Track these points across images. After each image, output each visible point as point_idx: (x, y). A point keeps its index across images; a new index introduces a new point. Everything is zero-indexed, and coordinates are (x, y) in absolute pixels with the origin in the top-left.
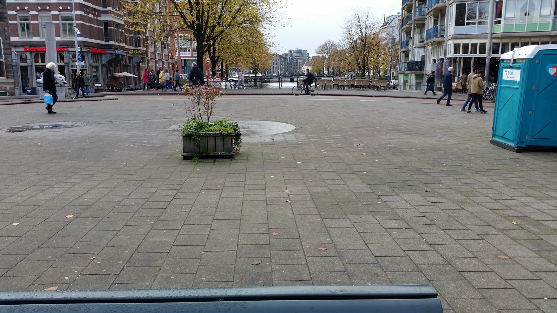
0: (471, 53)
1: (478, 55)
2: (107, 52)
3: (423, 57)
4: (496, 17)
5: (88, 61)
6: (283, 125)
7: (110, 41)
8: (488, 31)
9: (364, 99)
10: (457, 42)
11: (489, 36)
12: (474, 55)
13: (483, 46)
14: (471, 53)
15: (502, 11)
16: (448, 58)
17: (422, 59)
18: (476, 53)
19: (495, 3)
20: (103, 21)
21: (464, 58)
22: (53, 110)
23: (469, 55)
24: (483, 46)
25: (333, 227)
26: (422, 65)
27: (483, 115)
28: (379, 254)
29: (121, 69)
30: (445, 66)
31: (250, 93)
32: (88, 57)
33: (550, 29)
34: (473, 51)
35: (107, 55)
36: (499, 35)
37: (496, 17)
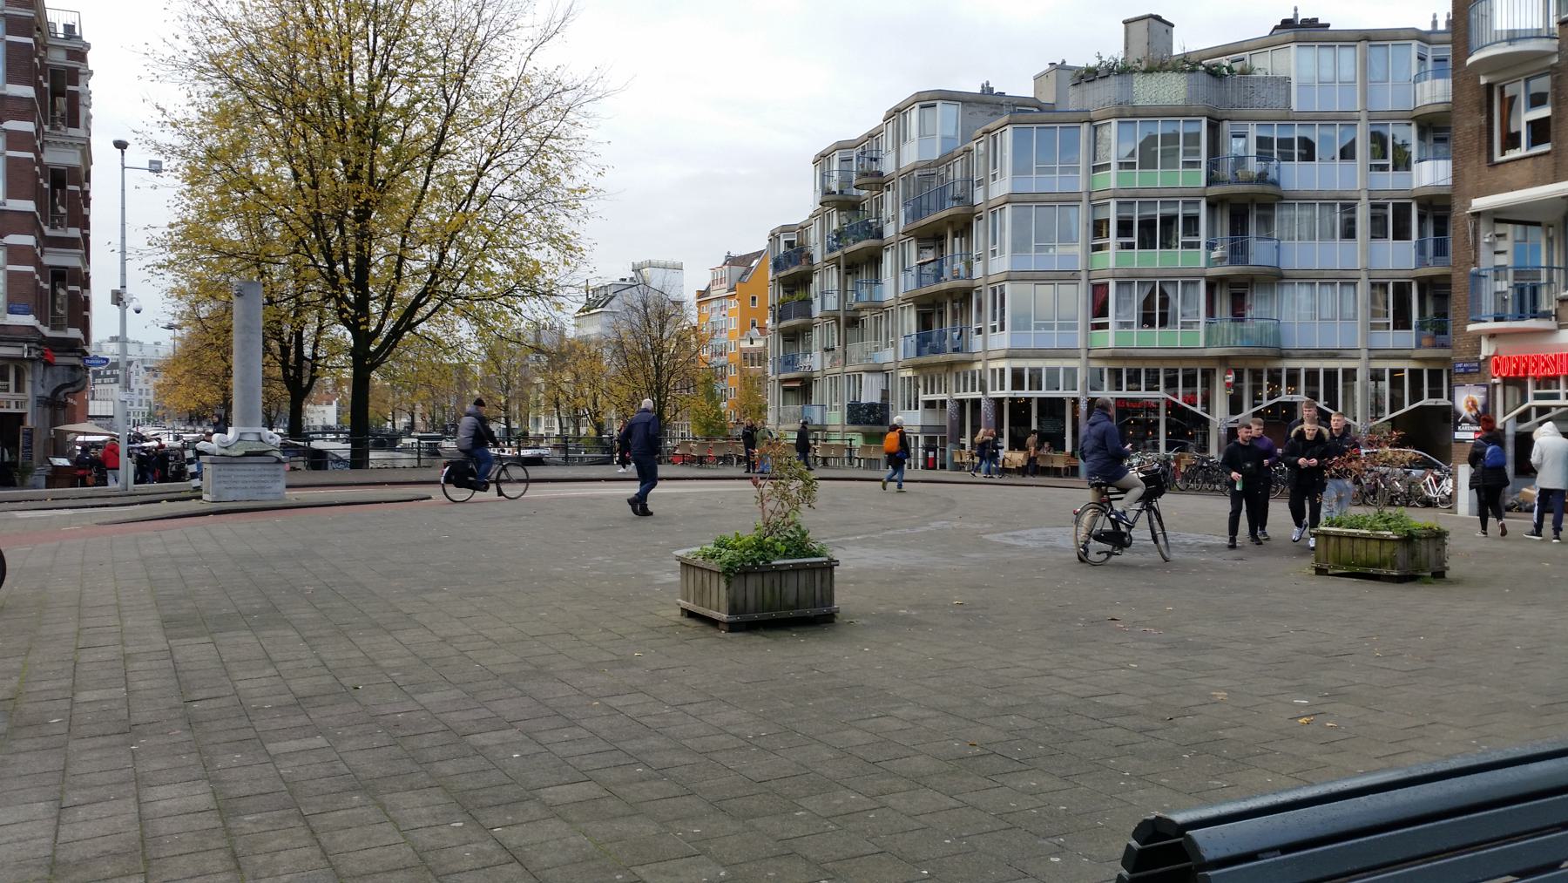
0: (1030, 389)
1: (1045, 393)
2: (58, 360)
3: (885, 393)
4: (1096, 315)
5: (33, 388)
6: (1241, 518)
7: (70, 330)
8: (1080, 344)
9: (688, 487)
10: (1018, 364)
11: (1083, 353)
12: (1035, 394)
13: (1070, 372)
14: (1030, 389)
15: (1108, 298)
16: (994, 399)
17: (882, 399)
18: (1022, 388)
19: (1090, 287)
20: (51, 267)
21: (1039, 398)
22: (650, 508)
23: (1025, 393)
24: (1070, 372)
25: (1027, 715)
26: (884, 413)
27: (644, 522)
28: (992, 757)
29: (933, 386)
30: (986, 414)
31: (414, 479)
32: (33, 376)
33: (1202, 345)
34: (1035, 385)
35: (57, 370)
36: (1107, 353)
37: (1096, 315)
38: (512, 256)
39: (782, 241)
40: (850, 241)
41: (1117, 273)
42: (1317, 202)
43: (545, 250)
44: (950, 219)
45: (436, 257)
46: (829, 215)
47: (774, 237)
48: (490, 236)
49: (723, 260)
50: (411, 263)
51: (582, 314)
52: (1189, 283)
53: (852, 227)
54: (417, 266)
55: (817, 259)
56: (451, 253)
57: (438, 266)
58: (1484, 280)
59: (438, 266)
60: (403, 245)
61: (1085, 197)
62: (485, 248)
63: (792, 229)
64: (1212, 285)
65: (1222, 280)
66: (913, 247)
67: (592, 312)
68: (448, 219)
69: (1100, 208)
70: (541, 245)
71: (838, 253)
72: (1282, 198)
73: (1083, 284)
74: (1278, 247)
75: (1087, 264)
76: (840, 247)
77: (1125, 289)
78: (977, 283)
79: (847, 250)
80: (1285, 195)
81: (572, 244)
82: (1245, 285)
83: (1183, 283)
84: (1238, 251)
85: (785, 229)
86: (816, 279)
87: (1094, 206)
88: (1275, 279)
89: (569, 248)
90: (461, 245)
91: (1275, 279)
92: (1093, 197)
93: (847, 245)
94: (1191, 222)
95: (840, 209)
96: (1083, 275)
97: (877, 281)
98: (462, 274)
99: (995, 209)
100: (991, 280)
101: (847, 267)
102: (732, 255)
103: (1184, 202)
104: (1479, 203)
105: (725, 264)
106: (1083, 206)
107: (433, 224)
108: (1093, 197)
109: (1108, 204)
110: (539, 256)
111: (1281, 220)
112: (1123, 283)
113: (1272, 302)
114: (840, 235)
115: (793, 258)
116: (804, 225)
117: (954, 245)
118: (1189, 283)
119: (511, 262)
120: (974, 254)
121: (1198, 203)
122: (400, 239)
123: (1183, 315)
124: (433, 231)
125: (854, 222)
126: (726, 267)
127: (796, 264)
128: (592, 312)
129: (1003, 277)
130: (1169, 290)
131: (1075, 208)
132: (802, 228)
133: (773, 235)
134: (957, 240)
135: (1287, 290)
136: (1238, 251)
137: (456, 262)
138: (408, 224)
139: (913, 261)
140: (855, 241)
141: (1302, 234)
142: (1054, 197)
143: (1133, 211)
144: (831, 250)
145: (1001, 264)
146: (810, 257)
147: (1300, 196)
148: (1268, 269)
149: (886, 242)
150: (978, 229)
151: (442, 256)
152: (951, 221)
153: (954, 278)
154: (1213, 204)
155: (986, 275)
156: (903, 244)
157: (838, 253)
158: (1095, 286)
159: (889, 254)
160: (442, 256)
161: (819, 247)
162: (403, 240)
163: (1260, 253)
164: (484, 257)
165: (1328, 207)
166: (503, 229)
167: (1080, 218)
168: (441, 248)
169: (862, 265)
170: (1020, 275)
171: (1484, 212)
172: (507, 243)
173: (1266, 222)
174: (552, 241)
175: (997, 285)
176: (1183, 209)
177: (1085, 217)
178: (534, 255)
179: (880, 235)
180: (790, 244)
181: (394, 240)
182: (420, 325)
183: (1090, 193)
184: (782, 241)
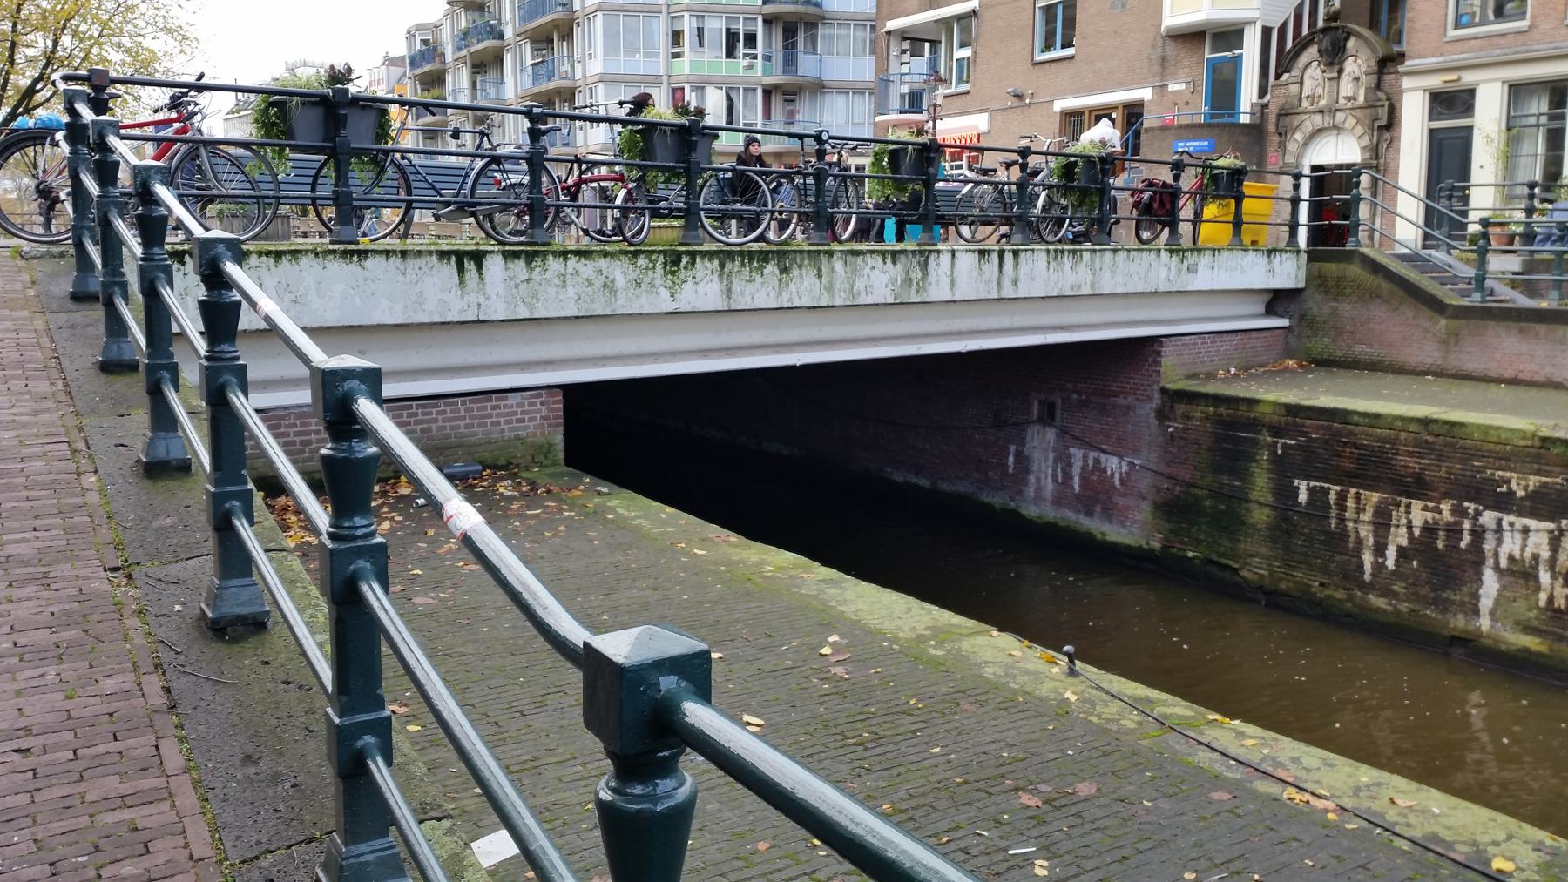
38: (129, 45)
39: (418, 39)
40: (475, 41)
41: (691, 78)
42: (852, 23)
43: (162, 41)
44: (556, 23)
45: (50, 43)
46: (589, 19)
47: (410, 36)
48: (104, 25)
49: (382, 61)
50: (24, 49)
51: (231, 116)
52: (750, 90)
53: (476, 27)
54: (30, 52)
55: (449, 58)
56: (66, 40)
57: (53, 52)
58: (891, 84)
59: (53, 52)
60: (14, 30)
61: (664, 9)
62: (100, 36)
63: (427, 27)
64: (768, 93)
65: (777, 87)
66: (528, 48)
67: (242, 113)
68: (60, 6)
69: (675, 20)
70: (158, 35)
71: (464, 53)
72: (824, 18)
73: (664, 87)
74: (820, 61)
75: (668, 70)
76: (466, 46)
77: (750, 94)
78: (578, 84)
79: (473, 49)
80: (826, 15)
81: (187, 34)
82: (794, 93)
83: (745, 89)
84: (790, 62)
85: (421, 28)
86: (449, 79)
87: (672, 18)
88: (818, 88)
89: (185, 38)
90: (75, 34)
91: (818, 88)
92: (671, 10)
93: (473, 44)
94: (751, 39)
95: (467, 10)
96: (665, 79)
97: (501, 81)
98: (79, 61)
99: (590, 16)
100: (589, 81)
101: (474, 66)
102: (391, 55)
103: (745, 18)
104: (891, 25)
105: (383, 64)
106: (663, 16)
107: (45, 10)
108: (671, 10)
109: (683, 16)
110: (156, 46)
111: (824, 37)
112: (697, 87)
113: (816, 104)
114: (466, 34)
115: (426, 56)
116: (438, 24)
117: (560, 48)
118: (750, 90)
119: (128, 51)
120: (575, 57)
121: (756, 19)
122: (11, 25)
123: (744, 117)
124: (45, 18)
125: (479, 22)
126: (384, 67)
127: (429, 62)
128: (242, 113)
129: (596, 79)
130: (734, 95)
131: (656, 19)
132: (436, 27)
133: (409, 33)
134: (565, 43)
135: (827, 97)
136: (790, 62)
137: (71, 51)
138: (19, 10)
139: (529, 61)
140: (479, 41)
141: (840, 50)
142: (639, 8)
143: (756, 26)
144: (460, 49)
145: (596, 67)
146: (443, 55)
147: (838, 17)
148: (809, 79)
149: (506, 43)
150: (577, 32)
151: (56, 43)
152: (555, 25)
153: (562, 78)
154: (769, 21)
155: (585, 77)
156: (520, 45)
157: (464, 53)
158: (675, 90)
159: (509, 55)
160: (56, 43)
161: (450, 45)
162: (15, 25)
163: (807, 65)
164: (100, 45)
165: (861, 27)
166: (117, 19)
167: (661, 29)
168: (55, 35)
169: (486, 64)
170: (612, 77)
171: (894, 30)
172: (122, 30)
173: (812, 41)
174: (168, 30)
175: (593, 86)
176: (744, 26)
177: (665, 28)
178: (148, 43)
179: (501, 36)
180: (425, 42)
181: (5, 27)
182: (38, 110)
183: (669, 6)
184: (418, 39)
